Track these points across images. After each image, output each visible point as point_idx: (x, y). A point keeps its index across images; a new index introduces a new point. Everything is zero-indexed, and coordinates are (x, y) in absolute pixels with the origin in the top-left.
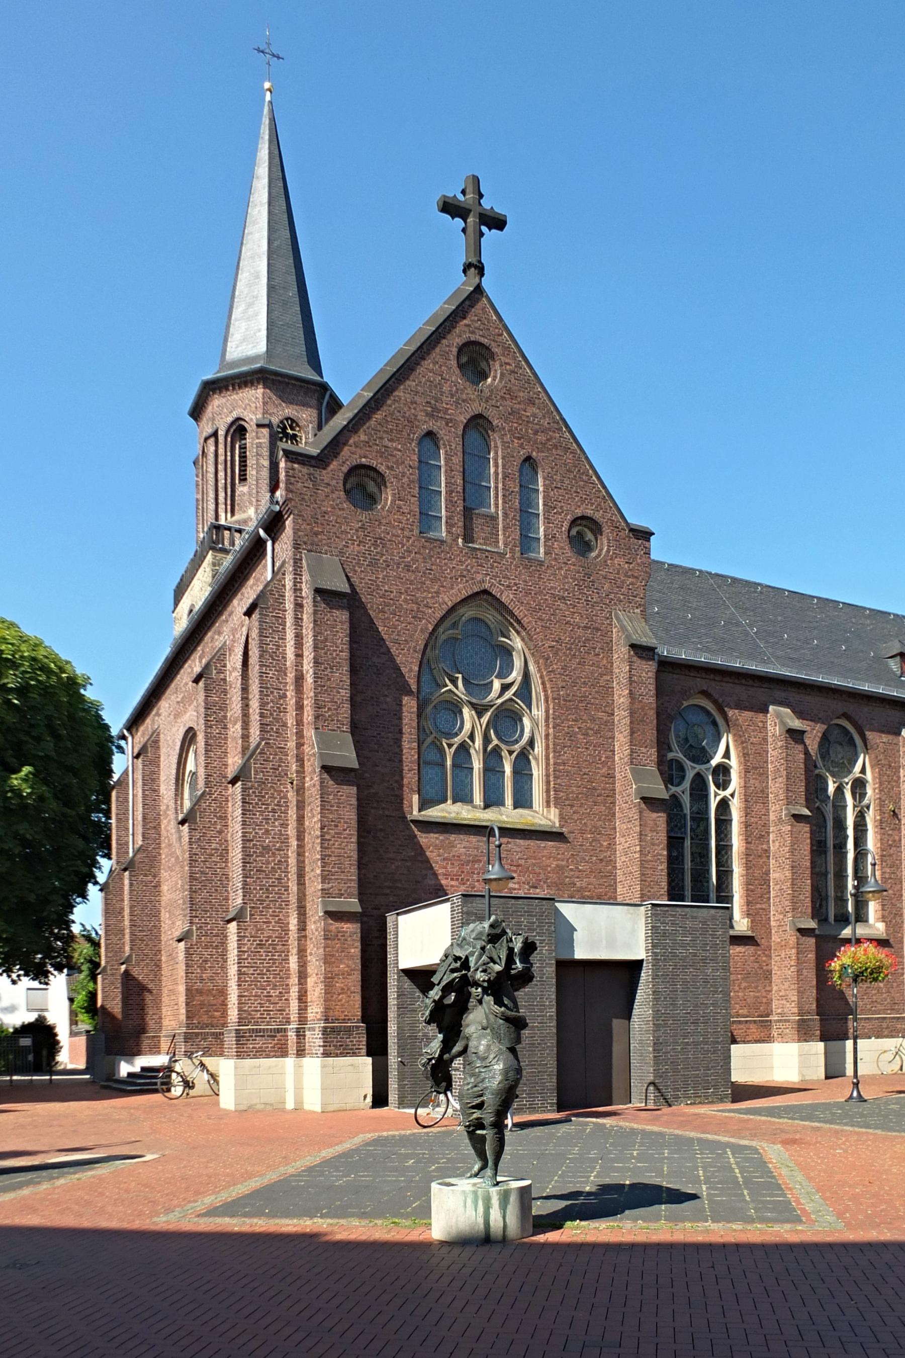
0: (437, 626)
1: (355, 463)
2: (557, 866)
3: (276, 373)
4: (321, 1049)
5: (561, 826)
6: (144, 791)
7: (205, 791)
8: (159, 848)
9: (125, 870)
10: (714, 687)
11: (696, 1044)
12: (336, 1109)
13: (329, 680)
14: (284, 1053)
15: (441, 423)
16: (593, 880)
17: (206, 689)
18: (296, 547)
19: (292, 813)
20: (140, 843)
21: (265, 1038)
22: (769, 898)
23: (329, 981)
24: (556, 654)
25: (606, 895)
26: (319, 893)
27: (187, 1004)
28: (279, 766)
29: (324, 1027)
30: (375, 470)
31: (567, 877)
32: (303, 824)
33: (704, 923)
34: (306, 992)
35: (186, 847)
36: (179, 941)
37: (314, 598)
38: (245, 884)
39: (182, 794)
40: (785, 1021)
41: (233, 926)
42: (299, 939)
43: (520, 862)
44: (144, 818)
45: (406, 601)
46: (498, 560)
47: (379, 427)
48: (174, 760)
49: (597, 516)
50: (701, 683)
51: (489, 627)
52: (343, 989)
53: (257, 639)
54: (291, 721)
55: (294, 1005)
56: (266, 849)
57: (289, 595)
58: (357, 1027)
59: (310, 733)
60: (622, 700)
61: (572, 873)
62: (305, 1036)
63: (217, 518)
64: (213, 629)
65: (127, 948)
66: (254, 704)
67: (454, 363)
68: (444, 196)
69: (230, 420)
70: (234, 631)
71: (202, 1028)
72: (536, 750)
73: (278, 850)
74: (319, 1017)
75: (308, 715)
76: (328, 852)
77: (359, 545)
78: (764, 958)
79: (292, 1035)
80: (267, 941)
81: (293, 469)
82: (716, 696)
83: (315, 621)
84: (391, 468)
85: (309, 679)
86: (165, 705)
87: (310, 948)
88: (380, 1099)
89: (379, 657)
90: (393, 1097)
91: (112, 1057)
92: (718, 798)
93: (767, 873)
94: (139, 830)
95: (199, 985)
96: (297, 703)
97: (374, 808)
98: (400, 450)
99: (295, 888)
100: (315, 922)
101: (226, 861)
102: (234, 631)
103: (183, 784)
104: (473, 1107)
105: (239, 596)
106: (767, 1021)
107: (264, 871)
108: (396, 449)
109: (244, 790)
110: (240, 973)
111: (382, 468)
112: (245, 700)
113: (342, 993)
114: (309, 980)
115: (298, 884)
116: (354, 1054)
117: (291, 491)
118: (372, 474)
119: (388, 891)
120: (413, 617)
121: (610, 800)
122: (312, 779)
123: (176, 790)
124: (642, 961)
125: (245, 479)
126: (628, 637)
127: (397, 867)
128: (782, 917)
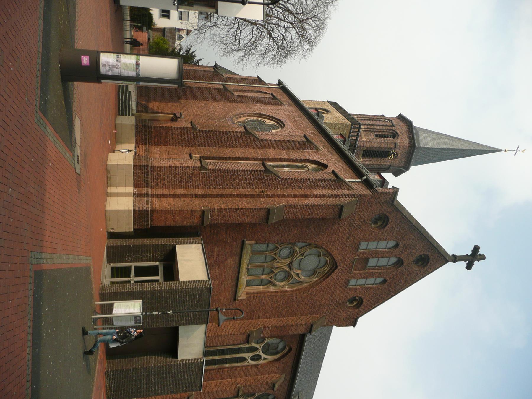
0: (324, 249)
2: (221, 299)
3: (413, 151)
6: (258, 97)
10: (292, 353)
14: (136, 186)
17: (301, 142)
18: (360, 196)
19: (249, 192)
21: (144, 175)
24: (310, 294)
26: (212, 207)
32: (244, 197)
34: (166, 198)
38: (218, 170)
44: (246, 97)
49: (362, 307)
51: (322, 267)
55: (159, 191)
56: (234, 180)
58: (148, 225)
59: (283, 202)
62: (144, 197)
69: (398, 132)
74: (154, 206)
75: (292, 201)
82: (289, 354)
83: (330, 205)
84: (386, 231)
87: (188, 200)
88: (112, 235)
92: (247, 357)
93: (214, 379)
95: (170, 133)
96: (297, 195)
101: (227, 147)
105: (340, 159)
109: (260, 171)
111: (387, 228)
114: (172, 199)
115: (217, 195)
116: (134, 224)
118: (385, 224)
121: (249, 318)
124: (177, 358)
126: (315, 322)
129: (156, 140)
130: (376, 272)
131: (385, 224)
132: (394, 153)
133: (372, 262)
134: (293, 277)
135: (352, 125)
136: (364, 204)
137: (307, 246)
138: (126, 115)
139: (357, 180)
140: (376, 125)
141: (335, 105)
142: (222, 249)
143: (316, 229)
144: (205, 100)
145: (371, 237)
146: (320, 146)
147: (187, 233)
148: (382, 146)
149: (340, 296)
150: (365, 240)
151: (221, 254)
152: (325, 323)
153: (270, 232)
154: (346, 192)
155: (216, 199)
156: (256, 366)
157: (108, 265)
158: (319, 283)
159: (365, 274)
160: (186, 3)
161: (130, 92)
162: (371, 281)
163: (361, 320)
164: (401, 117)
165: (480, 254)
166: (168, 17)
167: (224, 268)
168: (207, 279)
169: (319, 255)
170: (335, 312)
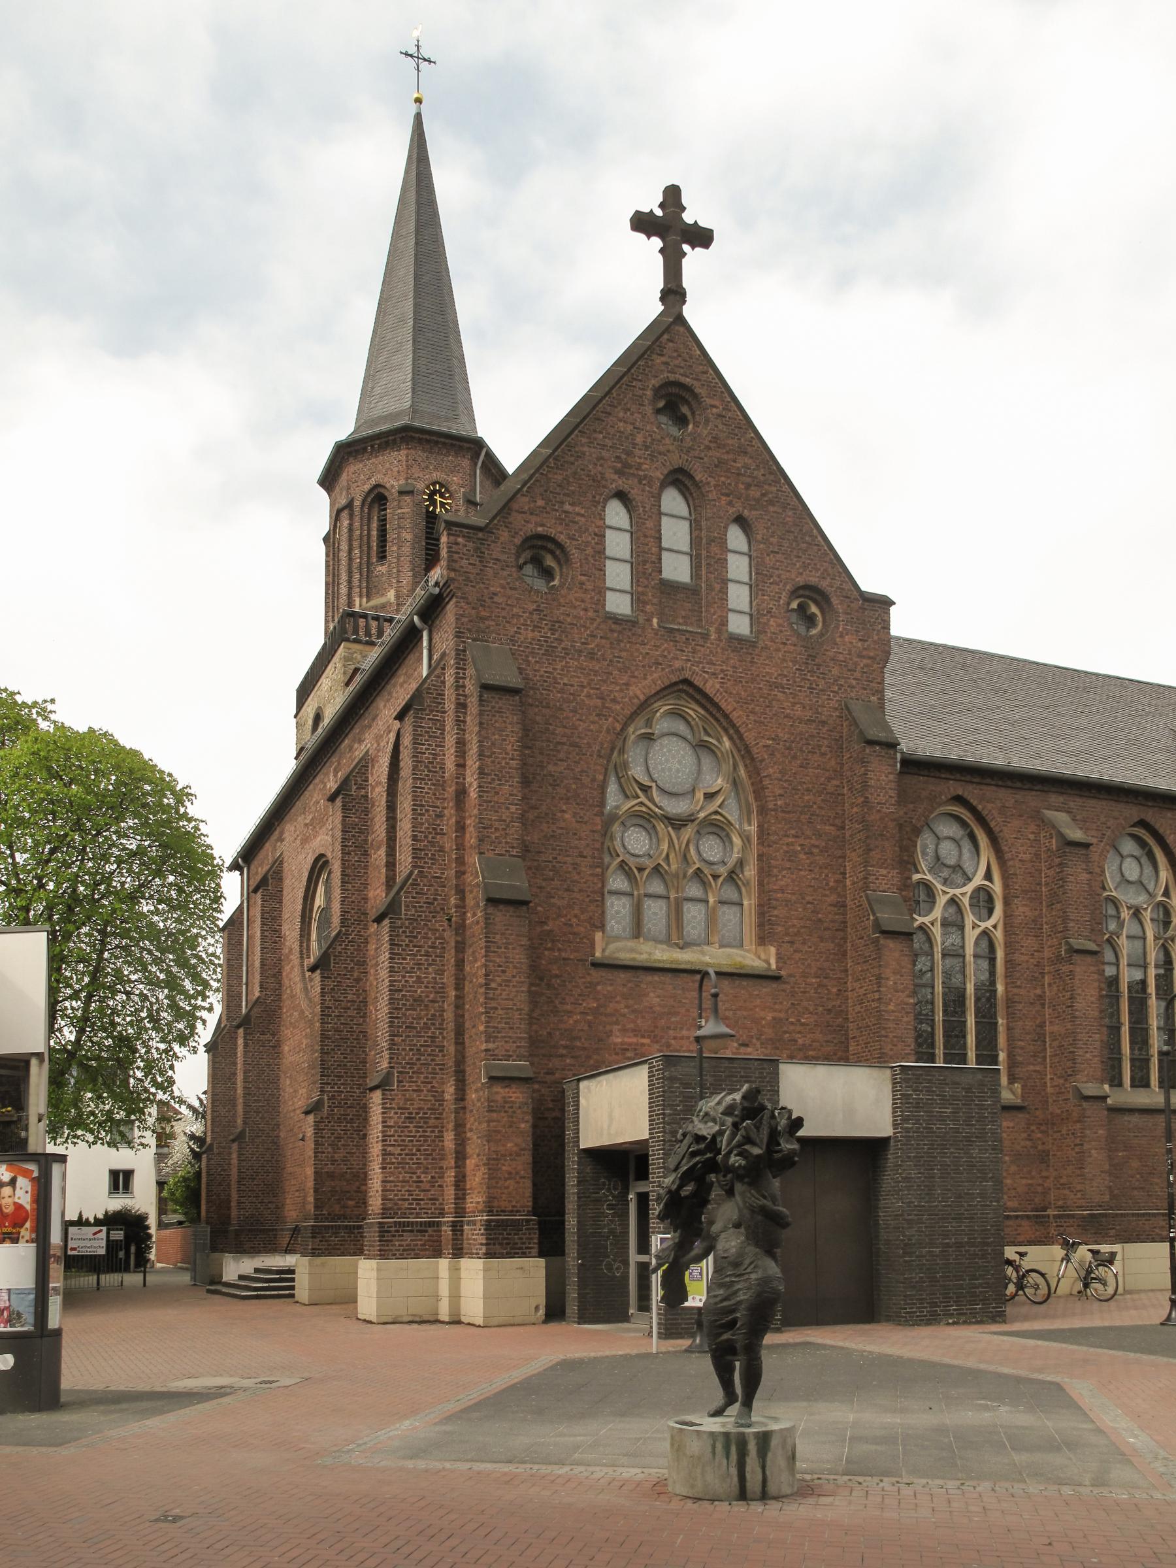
1: (529, 534)
2: (774, 1018)
4: (484, 1248)
5: (779, 968)
6: (263, 931)
7: (340, 931)
8: (280, 1000)
9: (238, 1027)
10: (972, 793)
11: (959, 1245)
12: (334, 1307)
13: (497, 793)
14: (437, 1253)
15: (633, 481)
16: (819, 1036)
17: (345, 808)
18: (458, 635)
20: (257, 994)
22: (1044, 1058)
23: (493, 1164)
25: (835, 1054)
27: (316, 1191)
28: (435, 899)
29: (487, 1221)
30: (553, 540)
31: (786, 1032)
32: (462, 970)
33: (968, 1090)
34: (464, 1177)
35: (317, 999)
36: (307, 1113)
37: (481, 696)
38: (392, 1043)
39: (309, 934)
40: (1069, 1216)
41: (377, 1096)
42: (457, 1112)
43: (727, 1013)
44: (263, 965)
45: (589, 696)
46: (701, 642)
47: (558, 490)
48: (301, 893)
49: (824, 585)
50: (955, 787)
52: (510, 1173)
53: (410, 747)
54: (449, 844)
55: (450, 1192)
57: (450, 694)
58: (528, 1221)
60: (855, 809)
61: (792, 1028)
62: (462, 1231)
63: (350, 603)
64: (350, 736)
65: (239, 1121)
66: (405, 827)
67: (649, 410)
68: (637, 212)
69: (367, 487)
70: (378, 738)
71: (333, 1220)
72: (747, 873)
73: (432, 1001)
74: (480, 1208)
76: (494, 1004)
77: (533, 631)
78: (1039, 1135)
79: (447, 1230)
80: (417, 1113)
81: (457, 544)
83: (481, 724)
84: (572, 538)
85: (473, 794)
86: (291, 829)
87: (471, 1122)
88: (554, 1312)
89: (556, 764)
90: (572, 1308)
91: (217, 1255)
92: (978, 931)
94: (257, 979)
96: (457, 822)
97: (549, 949)
98: (583, 516)
99: (452, 1049)
100: (476, 1091)
102: (378, 738)
103: (310, 923)
104: (722, 1326)
105: (385, 693)
106: (1044, 1216)
107: (415, 1028)
108: (578, 514)
109: (393, 929)
110: (385, 1153)
111: (562, 538)
112: (392, 820)
113: (509, 1178)
115: (456, 1043)
116: (524, 1255)
117: (454, 570)
118: (550, 546)
119: (564, 1052)
120: (598, 715)
122: (474, 915)
123: (302, 929)
124: (889, 1138)
125: (384, 557)
127: (576, 1021)
128: (1061, 1081)
129: (351, 1203)
130: (707, 553)
131: (550, 546)
132: (434, 493)
133: (676, 569)
134: (716, 813)
135: (348, 640)
136: (483, 619)
137: (619, 778)
138: (293, 1280)
139: (425, 644)
140: (350, 560)
141: (304, 692)
142: (617, 1023)
143: (561, 755)
144: (278, 1076)
145: (589, 586)
146: (359, 751)
147: (552, 1121)
148: (409, 537)
149: (784, 660)
150: (601, 602)
151: (632, 1026)
152: (874, 699)
153: (567, 890)
154: (449, 678)
155: (467, 1045)
156: (1007, 903)
157: (632, 1320)
158: (737, 731)
159: (710, 588)
160: (23, 1134)
161: (257, 1270)
162: (738, 567)
163: (868, 583)
164: (328, 480)
165: (661, 206)
166: (128, 1174)
167: (677, 1013)
168: (647, 1066)
169: (649, 738)
170: (835, 671)
